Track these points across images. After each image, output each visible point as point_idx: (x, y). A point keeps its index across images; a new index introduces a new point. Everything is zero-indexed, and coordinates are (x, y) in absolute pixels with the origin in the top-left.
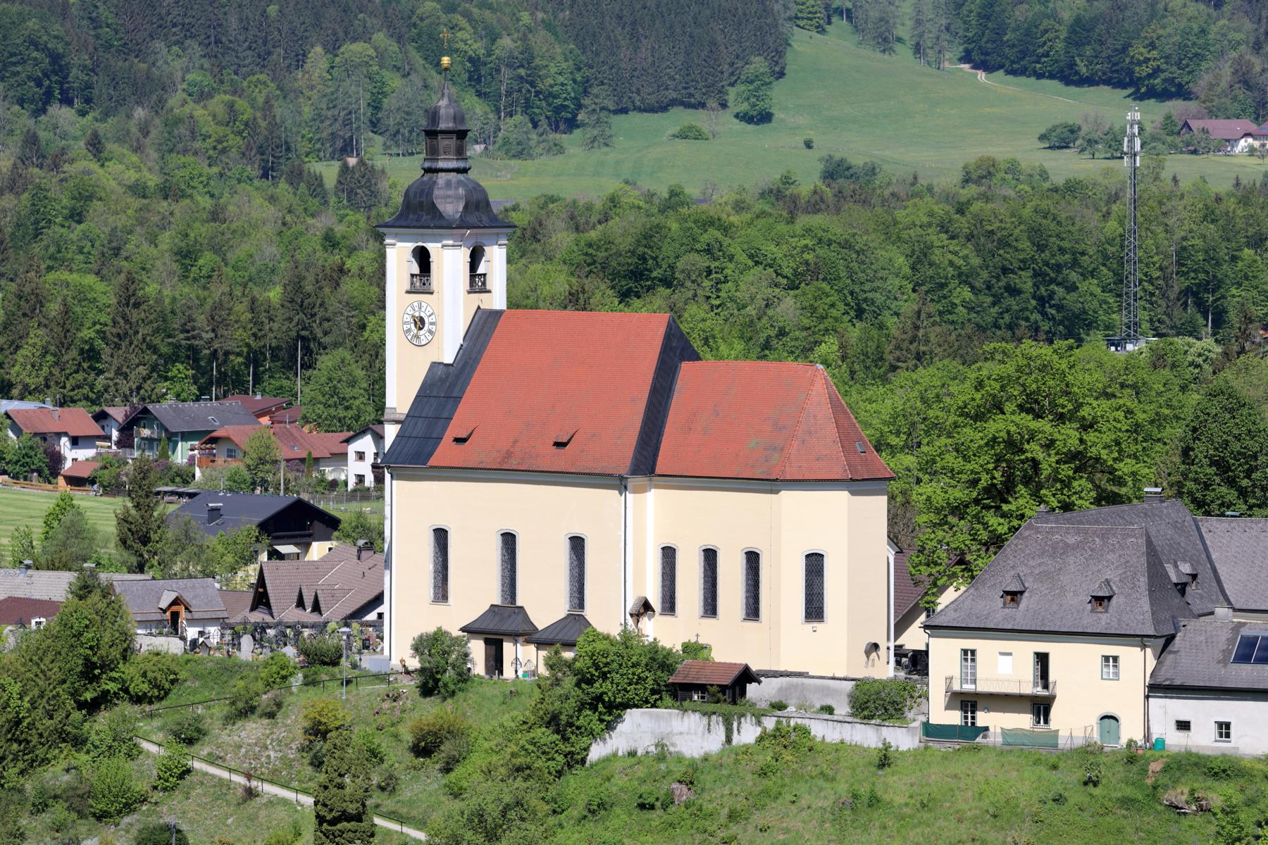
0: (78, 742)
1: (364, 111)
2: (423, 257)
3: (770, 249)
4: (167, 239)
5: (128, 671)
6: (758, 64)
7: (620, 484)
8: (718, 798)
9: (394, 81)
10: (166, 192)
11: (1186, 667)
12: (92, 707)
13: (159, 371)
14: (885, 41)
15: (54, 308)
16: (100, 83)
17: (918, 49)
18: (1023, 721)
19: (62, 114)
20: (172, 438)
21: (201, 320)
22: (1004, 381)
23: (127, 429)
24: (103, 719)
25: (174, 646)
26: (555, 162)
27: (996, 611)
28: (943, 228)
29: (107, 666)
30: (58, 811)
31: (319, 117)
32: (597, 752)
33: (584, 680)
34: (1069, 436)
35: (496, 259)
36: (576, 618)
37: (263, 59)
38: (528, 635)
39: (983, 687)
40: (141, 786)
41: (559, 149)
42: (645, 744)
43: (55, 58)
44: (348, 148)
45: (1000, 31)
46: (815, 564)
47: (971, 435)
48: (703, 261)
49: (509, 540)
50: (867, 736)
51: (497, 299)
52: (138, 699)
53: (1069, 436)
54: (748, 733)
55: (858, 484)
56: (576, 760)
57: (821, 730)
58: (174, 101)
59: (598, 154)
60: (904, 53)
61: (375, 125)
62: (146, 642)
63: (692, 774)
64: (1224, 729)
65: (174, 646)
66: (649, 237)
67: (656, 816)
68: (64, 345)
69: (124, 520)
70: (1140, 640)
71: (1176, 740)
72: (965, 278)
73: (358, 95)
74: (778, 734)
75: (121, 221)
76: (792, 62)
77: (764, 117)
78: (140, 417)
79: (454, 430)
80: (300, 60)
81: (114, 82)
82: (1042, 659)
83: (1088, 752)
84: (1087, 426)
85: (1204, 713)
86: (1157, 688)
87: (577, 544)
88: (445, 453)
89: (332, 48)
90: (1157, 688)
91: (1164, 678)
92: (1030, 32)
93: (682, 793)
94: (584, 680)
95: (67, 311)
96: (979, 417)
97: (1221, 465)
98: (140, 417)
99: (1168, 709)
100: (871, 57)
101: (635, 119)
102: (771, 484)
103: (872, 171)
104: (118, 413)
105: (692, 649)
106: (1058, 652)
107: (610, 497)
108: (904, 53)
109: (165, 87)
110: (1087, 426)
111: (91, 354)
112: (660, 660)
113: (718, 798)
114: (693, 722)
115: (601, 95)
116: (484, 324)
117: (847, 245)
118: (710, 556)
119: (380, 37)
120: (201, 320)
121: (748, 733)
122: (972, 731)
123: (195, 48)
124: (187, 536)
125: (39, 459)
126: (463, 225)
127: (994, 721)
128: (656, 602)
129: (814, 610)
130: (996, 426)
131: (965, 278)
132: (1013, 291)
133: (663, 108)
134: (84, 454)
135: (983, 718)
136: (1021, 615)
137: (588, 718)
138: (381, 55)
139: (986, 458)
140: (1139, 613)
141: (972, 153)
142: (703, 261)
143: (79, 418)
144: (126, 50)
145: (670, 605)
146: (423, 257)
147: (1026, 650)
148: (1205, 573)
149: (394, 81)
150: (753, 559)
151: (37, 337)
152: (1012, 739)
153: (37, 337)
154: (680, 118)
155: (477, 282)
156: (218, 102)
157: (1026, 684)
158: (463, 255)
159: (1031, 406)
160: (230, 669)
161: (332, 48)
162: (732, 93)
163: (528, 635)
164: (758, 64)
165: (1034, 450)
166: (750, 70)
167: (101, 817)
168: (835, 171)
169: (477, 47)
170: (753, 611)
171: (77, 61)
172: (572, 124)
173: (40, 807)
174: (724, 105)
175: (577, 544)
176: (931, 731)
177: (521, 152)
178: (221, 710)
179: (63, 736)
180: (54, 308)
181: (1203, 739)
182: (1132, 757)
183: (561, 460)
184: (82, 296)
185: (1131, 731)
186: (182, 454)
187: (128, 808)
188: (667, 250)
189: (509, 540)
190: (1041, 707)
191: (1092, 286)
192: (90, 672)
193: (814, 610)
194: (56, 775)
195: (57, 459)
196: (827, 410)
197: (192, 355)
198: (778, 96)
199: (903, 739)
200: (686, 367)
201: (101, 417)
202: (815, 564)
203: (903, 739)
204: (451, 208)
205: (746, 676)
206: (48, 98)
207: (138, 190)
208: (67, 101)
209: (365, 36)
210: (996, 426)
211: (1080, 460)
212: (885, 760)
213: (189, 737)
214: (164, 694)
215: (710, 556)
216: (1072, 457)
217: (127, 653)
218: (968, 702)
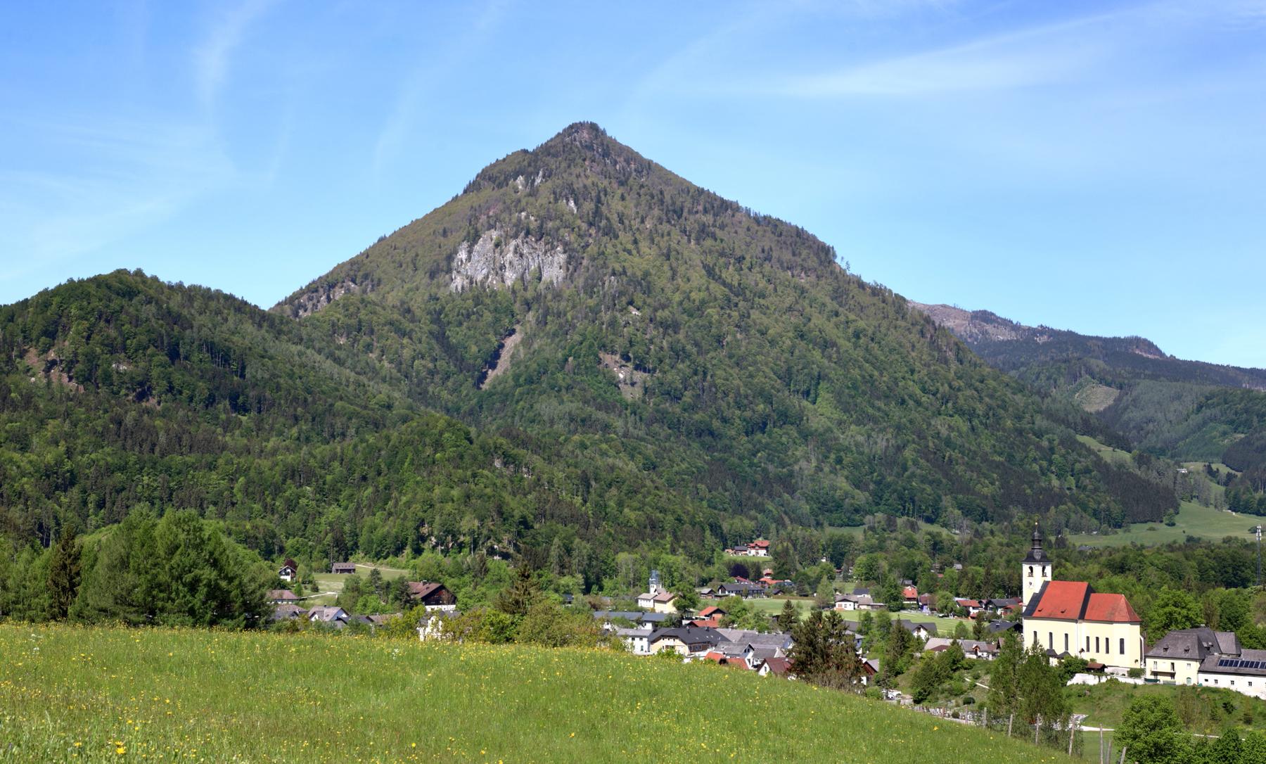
0: (951, 678)
1: (1063, 522)
2: (1031, 568)
3: (1156, 562)
4: (1005, 558)
5: (963, 662)
6: (1171, 511)
7: (1076, 622)
8: (1096, 694)
9: (1073, 515)
10: (1008, 545)
11: (1207, 666)
12: (955, 670)
13: (995, 591)
14: (1207, 505)
15: (970, 575)
16: (995, 515)
17: (1216, 507)
18: (1168, 679)
19: (986, 524)
20: (997, 608)
21: (1006, 579)
22: (1169, 599)
23: (986, 605)
24: (957, 673)
25: (974, 657)
26: (1116, 536)
27: (1162, 652)
28: (1207, 556)
29: (958, 661)
30: (946, 694)
31: (1052, 525)
32: (1069, 683)
33: (1066, 666)
34: (1184, 612)
35: (1049, 569)
36: (1066, 653)
37: (1038, 509)
38: (1055, 656)
39: (1159, 670)
40: (965, 688)
41: (1116, 533)
42: (1080, 682)
43: (984, 510)
44: (1059, 533)
45: (1239, 502)
46: (1122, 641)
47: (1161, 611)
48: (1138, 565)
49: (1051, 634)
50: (1131, 681)
51: (1049, 578)
52: (966, 669)
53: (1184, 612)
54: (1104, 680)
55: (1132, 622)
56: (1064, 685)
57: (1122, 680)
58: (1014, 520)
59: (1127, 534)
60: (1212, 507)
61: (1067, 526)
62: (968, 655)
63: (1091, 688)
64: (1216, 681)
65: (974, 657)
66: (1124, 558)
67: (1082, 699)
68: (973, 584)
69: (975, 628)
70: (1196, 660)
71: (1205, 684)
72: (1213, 569)
73: (1063, 520)
74: (1111, 679)
75: (995, 552)
76: (1181, 510)
77: (1173, 525)
78: (989, 602)
79: (1038, 608)
80: (1048, 510)
81: (999, 516)
82: (1173, 664)
83: (1184, 686)
84: (1189, 610)
85: (1211, 677)
86: (1200, 671)
87: (1066, 635)
88: (1036, 614)
89: (1057, 507)
90: (1200, 671)
91: (1203, 669)
92: (1247, 502)
93: (1088, 693)
94: (1066, 666)
95: (973, 576)
96: (1163, 607)
97: (1229, 620)
98: (989, 602)
99: (1203, 676)
100: (1203, 508)
101: (1138, 525)
102: (1111, 622)
103: (1199, 539)
104: (984, 601)
105: (1092, 660)
106: (1175, 662)
107: (1073, 624)
108: (1212, 507)
109: (1012, 517)
110: (1189, 610)
111: (979, 587)
112: (1084, 662)
113: (1096, 694)
114: (1091, 677)
115: (1128, 519)
116: (1046, 584)
117: (1176, 561)
118: (1097, 639)
119: (1069, 504)
120: (1006, 579)
121: (1104, 680)
122: (1156, 680)
123: (1020, 507)
124: (989, 632)
125: (964, 612)
126: (1040, 561)
127: (1162, 679)
128: (1085, 649)
129: (1122, 652)
130: (1167, 609)
131: (1213, 569)
132: (1226, 572)
133: (1146, 522)
134: (976, 611)
135: (1159, 677)
136: (1167, 654)
137: (1067, 676)
138: (1069, 509)
139: (1164, 617)
140: (1196, 653)
141: (1225, 535)
142: (1138, 565)
143: (975, 603)
144: (1002, 508)
145: (1088, 650)
146: (1031, 568)
147: (1169, 662)
148: (1215, 645)
149: (1073, 515)
150: (1107, 639)
151: (965, 582)
152: (1166, 684)
153: (965, 582)
154: (1150, 525)
155: (1044, 574)
156: (1025, 521)
157: (1169, 670)
158: (1041, 568)
159: (1175, 605)
160: (987, 662)
161: (1057, 507)
162: (1164, 518)
163: (1055, 656)
164: (1171, 511)
165: (1176, 615)
166: (1168, 512)
167: (956, 695)
168: (1190, 539)
169: (1095, 506)
170: (1107, 652)
171: (990, 510)
172: (1120, 527)
173: (942, 693)
174: (1161, 522)
175: (1066, 635)
176: (1146, 680)
177: (1106, 534)
178: (984, 672)
179: (948, 677)
180: (970, 575)
181: (1211, 684)
182: (1194, 687)
183: (1063, 616)
184: (977, 572)
185: (1194, 682)
186: (999, 612)
187: (962, 693)
188: (1129, 561)
189: (1051, 634)
190: (1172, 675)
191: (1248, 571)
192: (954, 662)
193: (1122, 652)
194: (946, 685)
195: (969, 612)
196: (1124, 605)
197: (1004, 587)
198: (1177, 519)
199: (1140, 682)
200: (1092, 595)
201: (980, 602)
202: (1122, 641)
203: (1140, 682)
204: (1038, 557)
205: (1104, 667)
206: (982, 520)
207: (1001, 544)
208: (987, 520)
209: (1065, 503)
210: (1167, 609)
211: (1188, 618)
212: (1135, 686)
213: (977, 678)
214: (971, 668)
215: (1097, 639)
216: (1184, 617)
217: (963, 657)
218: (1155, 673)
